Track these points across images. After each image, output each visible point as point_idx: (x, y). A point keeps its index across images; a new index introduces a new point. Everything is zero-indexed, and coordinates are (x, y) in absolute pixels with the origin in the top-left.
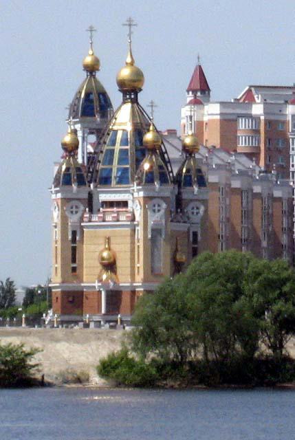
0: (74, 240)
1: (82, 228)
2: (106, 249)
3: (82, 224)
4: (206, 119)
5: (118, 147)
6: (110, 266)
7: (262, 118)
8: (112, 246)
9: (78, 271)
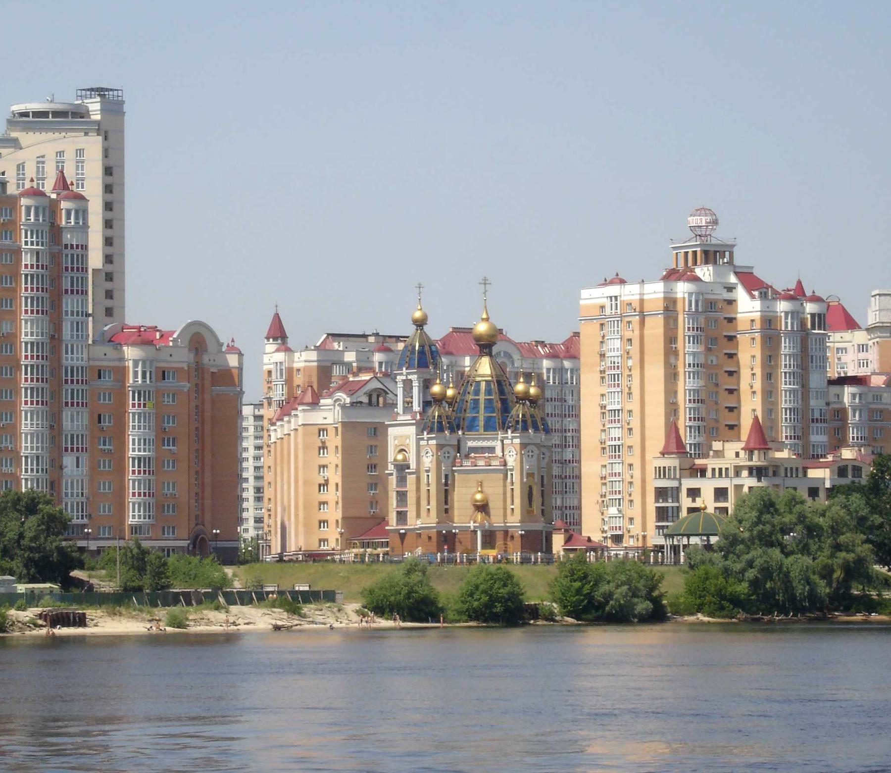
0: (446, 484)
1: (453, 471)
2: (479, 492)
3: (454, 468)
4: (296, 365)
5: (482, 397)
6: (483, 508)
7: (355, 365)
8: (485, 489)
9: (450, 512)
